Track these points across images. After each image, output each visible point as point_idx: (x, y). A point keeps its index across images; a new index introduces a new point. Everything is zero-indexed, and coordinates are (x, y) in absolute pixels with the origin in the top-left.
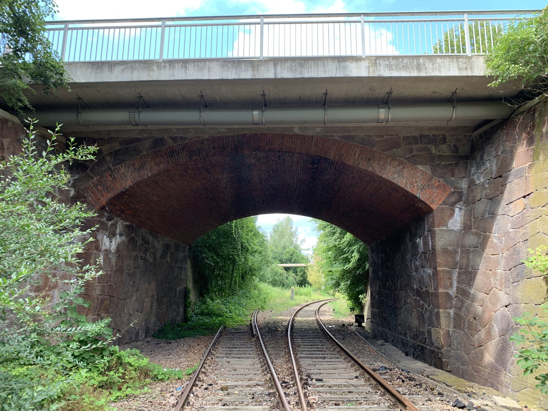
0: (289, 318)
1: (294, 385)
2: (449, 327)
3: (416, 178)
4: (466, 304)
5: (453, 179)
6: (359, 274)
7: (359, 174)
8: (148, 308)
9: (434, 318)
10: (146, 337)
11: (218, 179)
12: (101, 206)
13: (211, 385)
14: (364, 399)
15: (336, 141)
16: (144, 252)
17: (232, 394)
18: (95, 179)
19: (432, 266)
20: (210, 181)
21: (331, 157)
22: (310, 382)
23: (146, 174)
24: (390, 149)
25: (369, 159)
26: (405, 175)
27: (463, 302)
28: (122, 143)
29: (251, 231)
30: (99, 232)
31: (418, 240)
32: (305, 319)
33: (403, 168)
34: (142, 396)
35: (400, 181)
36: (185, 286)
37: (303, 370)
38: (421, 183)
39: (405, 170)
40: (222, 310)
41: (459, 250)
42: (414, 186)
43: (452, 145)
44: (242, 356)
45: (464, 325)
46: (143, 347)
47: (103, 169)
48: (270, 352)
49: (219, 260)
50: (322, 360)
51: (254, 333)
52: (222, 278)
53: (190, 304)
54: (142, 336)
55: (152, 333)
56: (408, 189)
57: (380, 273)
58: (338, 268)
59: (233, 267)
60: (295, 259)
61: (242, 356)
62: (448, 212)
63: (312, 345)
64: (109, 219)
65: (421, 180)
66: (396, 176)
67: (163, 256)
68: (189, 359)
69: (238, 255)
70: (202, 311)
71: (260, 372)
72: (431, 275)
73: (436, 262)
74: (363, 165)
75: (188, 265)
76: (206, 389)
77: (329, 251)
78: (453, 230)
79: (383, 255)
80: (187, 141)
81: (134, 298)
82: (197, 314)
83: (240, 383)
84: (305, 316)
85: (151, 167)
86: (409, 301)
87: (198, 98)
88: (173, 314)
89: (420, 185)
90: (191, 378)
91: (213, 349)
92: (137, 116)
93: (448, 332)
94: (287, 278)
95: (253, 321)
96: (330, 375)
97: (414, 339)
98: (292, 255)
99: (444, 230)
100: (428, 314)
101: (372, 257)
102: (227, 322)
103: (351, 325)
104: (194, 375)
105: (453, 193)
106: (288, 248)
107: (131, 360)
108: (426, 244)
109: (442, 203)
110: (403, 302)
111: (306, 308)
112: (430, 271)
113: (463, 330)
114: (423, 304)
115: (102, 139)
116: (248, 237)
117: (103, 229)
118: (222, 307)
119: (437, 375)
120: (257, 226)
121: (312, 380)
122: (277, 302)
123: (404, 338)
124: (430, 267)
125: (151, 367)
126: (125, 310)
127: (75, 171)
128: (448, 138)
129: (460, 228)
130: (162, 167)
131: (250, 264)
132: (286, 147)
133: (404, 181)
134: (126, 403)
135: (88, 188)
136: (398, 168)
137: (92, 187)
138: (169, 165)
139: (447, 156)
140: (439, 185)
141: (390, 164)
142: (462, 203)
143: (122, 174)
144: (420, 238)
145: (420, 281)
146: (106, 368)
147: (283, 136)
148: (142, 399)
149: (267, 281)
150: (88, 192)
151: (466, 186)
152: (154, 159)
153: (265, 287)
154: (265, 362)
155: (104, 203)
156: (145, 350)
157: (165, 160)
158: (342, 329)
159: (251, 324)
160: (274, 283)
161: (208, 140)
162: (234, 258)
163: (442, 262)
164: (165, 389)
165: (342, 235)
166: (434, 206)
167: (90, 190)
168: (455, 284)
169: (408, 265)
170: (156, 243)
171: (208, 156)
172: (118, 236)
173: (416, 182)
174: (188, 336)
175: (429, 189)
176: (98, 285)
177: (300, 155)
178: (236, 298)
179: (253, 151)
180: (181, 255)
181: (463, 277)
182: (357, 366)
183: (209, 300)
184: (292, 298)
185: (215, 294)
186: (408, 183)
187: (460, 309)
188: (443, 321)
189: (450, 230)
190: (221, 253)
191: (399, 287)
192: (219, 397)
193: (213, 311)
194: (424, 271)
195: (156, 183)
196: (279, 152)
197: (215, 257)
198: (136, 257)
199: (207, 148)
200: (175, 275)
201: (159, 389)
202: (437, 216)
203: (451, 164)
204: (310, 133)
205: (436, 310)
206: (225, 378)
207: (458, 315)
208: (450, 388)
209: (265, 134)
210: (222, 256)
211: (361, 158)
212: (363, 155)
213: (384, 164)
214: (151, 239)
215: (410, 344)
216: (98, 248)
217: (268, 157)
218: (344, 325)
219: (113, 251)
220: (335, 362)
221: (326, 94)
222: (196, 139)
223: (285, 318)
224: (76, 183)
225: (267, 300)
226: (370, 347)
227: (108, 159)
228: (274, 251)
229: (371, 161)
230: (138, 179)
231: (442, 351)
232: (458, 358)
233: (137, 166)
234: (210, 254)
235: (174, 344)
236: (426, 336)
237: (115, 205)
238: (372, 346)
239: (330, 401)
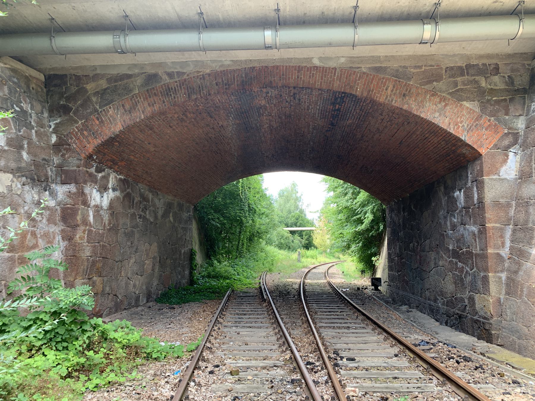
0: (298, 281)
1: (322, 369)
2: (500, 294)
3: (461, 117)
4: (524, 267)
5: (507, 117)
6: (372, 236)
7: (391, 114)
8: (150, 271)
9: (480, 283)
10: (147, 302)
11: (222, 126)
12: (87, 154)
13: (217, 366)
14: (419, 390)
15: (364, 73)
16: (143, 210)
17: (245, 380)
18: (80, 123)
19: (478, 222)
20: (213, 128)
21: (358, 93)
22: (340, 362)
23: (139, 115)
24: (430, 82)
25: (404, 95)
26: (448, 114)
27: (520, 265)
28: (109, 80)
29: (258, 193)
30: (86, 184)
31: (457, 193)
32: (315, 281)
33: (446, 105)
34: (128, 384)
35: (441, 121)
36: (191, 248)
37: (328, 344)
38: (467, 123)
39: (448, 108)
40: (230, 272)
41: (514, 203)
42: (459, 127)
43: (506, 76)
44: (253, 324)
45: (522, 291)
46: (143, 313)
47: (89, 111)
48: (285, 320)
49: (226, 221)
50: (346, 331)
51: (265, 297)
52: (230, 241)
53: (196, 266)
54: (143, 301)
55: (155, 297)
56: (452, 131)
57: (401, 234)
58: (349, 230)
59: (240, 229)
60: (301, 223)
61: (253, 324)
62: (500, 158)
63: (330, 312)
64: (99, 170)
65: (468, 119)
66: (437, 114)
67: (165, 215)
68: (193, 329)
69: (245, 217)
70: (209, 273)
71: (276, 346)
72: (476, 232)
73: (484, 218)
74: (397, 102)
75: (194, 226)
76: (211, 372)
77: (340, 213)
78: (506, 179)
79: (406, 214)
80: (185, 77)
81: (132, 261)
82: (203, 277)
83: (253, 363)
84: (314, 279)
85: (144, 107)
86: (441, 263)
87: (197, 17)
88: (178, 277)
89: (466, 126)
90: (192, 357)
91: (220, 317)
92: (122, 39)
93: (499, 300)
94: (293, 241)
95: (262, 284)
96: (362, 351)
97: (447, 306)
98: (297, 219)
99: (495, 180)
100: (469, 278)
101: (391, 217)
102: (235, 285)
103: (365, 289)
104: (197, 353)
105: (507, 135)
106: (294, 212)
107: (118, 335)
108: (468, 197)
109: (493, 147)
110: (432, 265)
111: (314, 270)
112: (474, 229)
113: (521, 297)
114: (463, 267)
115: (86, 76)
116: (255, 199)
117: (92, 181)
118: (230, 269)
119: (493, 353)
120: (263, 188)
121: (341, 360)
122: (282, 265)
123: (432, 303)
124: (475, 223)
125: (144, 343)
126: (123, 273)
127: (57, 114)
128: (502, 68)
129: (514, 177)
130: (156, 107)
131: (257, 225)
132: (303, 81)
133: (447, 120)
134: (106, 394)
135: (72, 133)
136: (439, 106)
137: (76, 133)
138: (165, 105)
139: (500, 90)
140: (489, 126)
141: (430, 100)
142: (517, 146)
143: (111, 116)
144: (460, 190)
145: (458, 241)
146: (85, 346)
147: (299, 69)
148: (128, 388)
149: (274, 244)
150: (72, 138)
151: (523, 126)
152: (147, 98)
153: (272, 250)
154: (281, 333)
155: (91, 150)
156: (144, 317)
157: (160, 99)
158: (358, 292)
159: (260, 287)
160: (281, 246)
161: (209, 75)
162: (241, 220)
163: (492, 217)
164: (159, 373)
165: (355, 195)
166: (483, 151)
167: (74, 136)
168: (508, 244)
169: (440, 223)
170: (156, 201)
171: (210, 95)
172: (111, 190)
173: (461, 122)
174: (194, 301)
175: (477, 130)
176: (87, 245)
177: (320, 92)
178: (244, 260)
179: (263, 88)
180: (185, 215)
181: (520, 235)
182: (391, 339)
183: (216, 262)
184: (299, 261)
185: (223, 256)
186: (452, 124)
187: (516, 272)
188: (493, 287)
189: (502, 180)
190: (227, 215)
191: (427, 248)
192: (228, 385)
193: (221, 273)
194: (465, 229)
195: (151, 129)
196: (294, 88)
197: (222, 219)
198: (133, 215)
199: (208, 84)
200: (179, 236)
201: (152, 372)
202: (487, 163)
203: (505, 100)
204: (332, 64)
205: (482, 274)
206: (235, 356)
207: (513, 280)
208: (519, 372)
209: (277, 67)
210: (229, 217)
211: (395, 94)
212: (396, 90)
213: (422, 101)
214: (150, 196)
215: (442, 311)
216: (85, 203)
217: (281, 96)
218: (358, 289)
219: (105, 208)
220: (363, 333)
221: (356, 7)
222: (196, 74)
223: (294, 281)
224: (58, 127)
225: (274, 262)
226: (395, 315)
227: (94, 99)
228: (280, 215)
229: (407, 98)
230: (129, 122)
231: (491, 321)
232: (514, 331)
233: (127, 107)
234: (216, 216)
235: (178, 310)
236: (466, 304)
237: (105, 154)
238: (397, 313)
239: (374, 392)
